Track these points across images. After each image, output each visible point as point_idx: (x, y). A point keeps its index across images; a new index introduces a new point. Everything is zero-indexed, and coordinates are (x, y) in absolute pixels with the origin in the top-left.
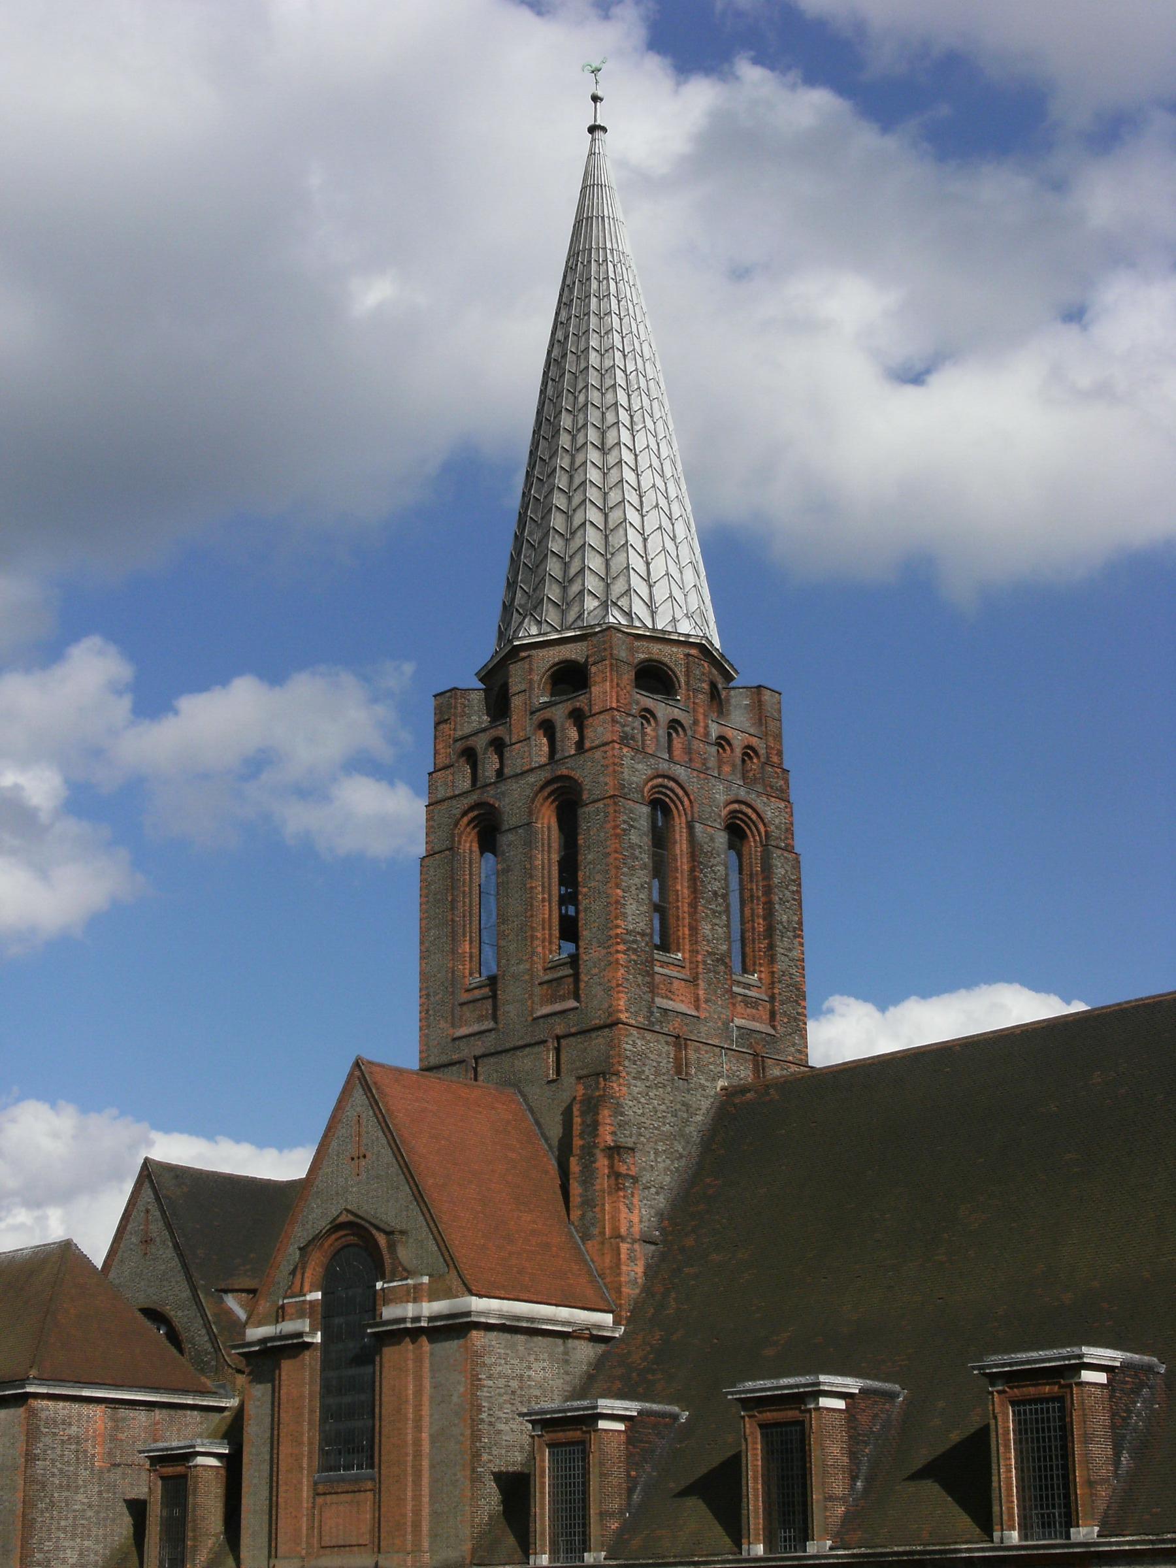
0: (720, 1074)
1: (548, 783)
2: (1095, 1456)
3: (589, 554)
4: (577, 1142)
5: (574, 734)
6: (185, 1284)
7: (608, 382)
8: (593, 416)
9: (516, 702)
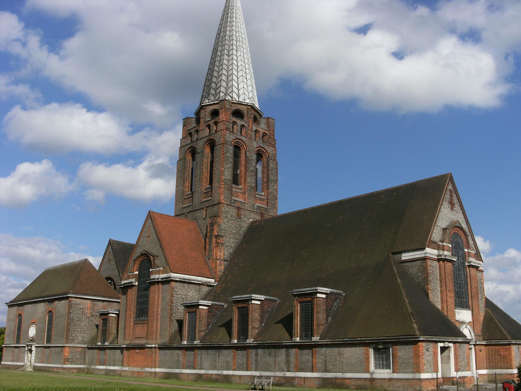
0: (249, 218)
1: (208, 141)
2: (320, 317)
3: (222, 82)
4: (208, 234)
5: (215, 128)
6: (117, 271)
7: (231, 39)
8: (226, 47)
9: (202, 120)
